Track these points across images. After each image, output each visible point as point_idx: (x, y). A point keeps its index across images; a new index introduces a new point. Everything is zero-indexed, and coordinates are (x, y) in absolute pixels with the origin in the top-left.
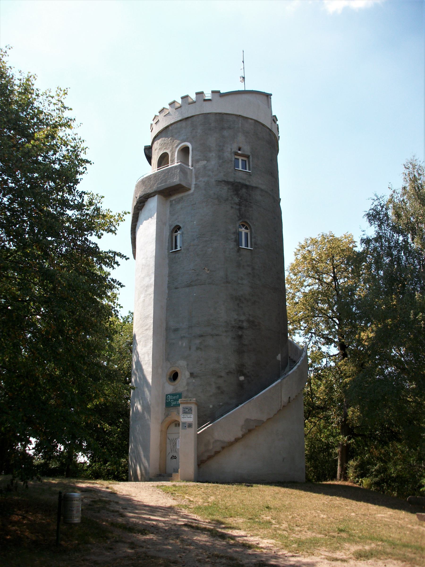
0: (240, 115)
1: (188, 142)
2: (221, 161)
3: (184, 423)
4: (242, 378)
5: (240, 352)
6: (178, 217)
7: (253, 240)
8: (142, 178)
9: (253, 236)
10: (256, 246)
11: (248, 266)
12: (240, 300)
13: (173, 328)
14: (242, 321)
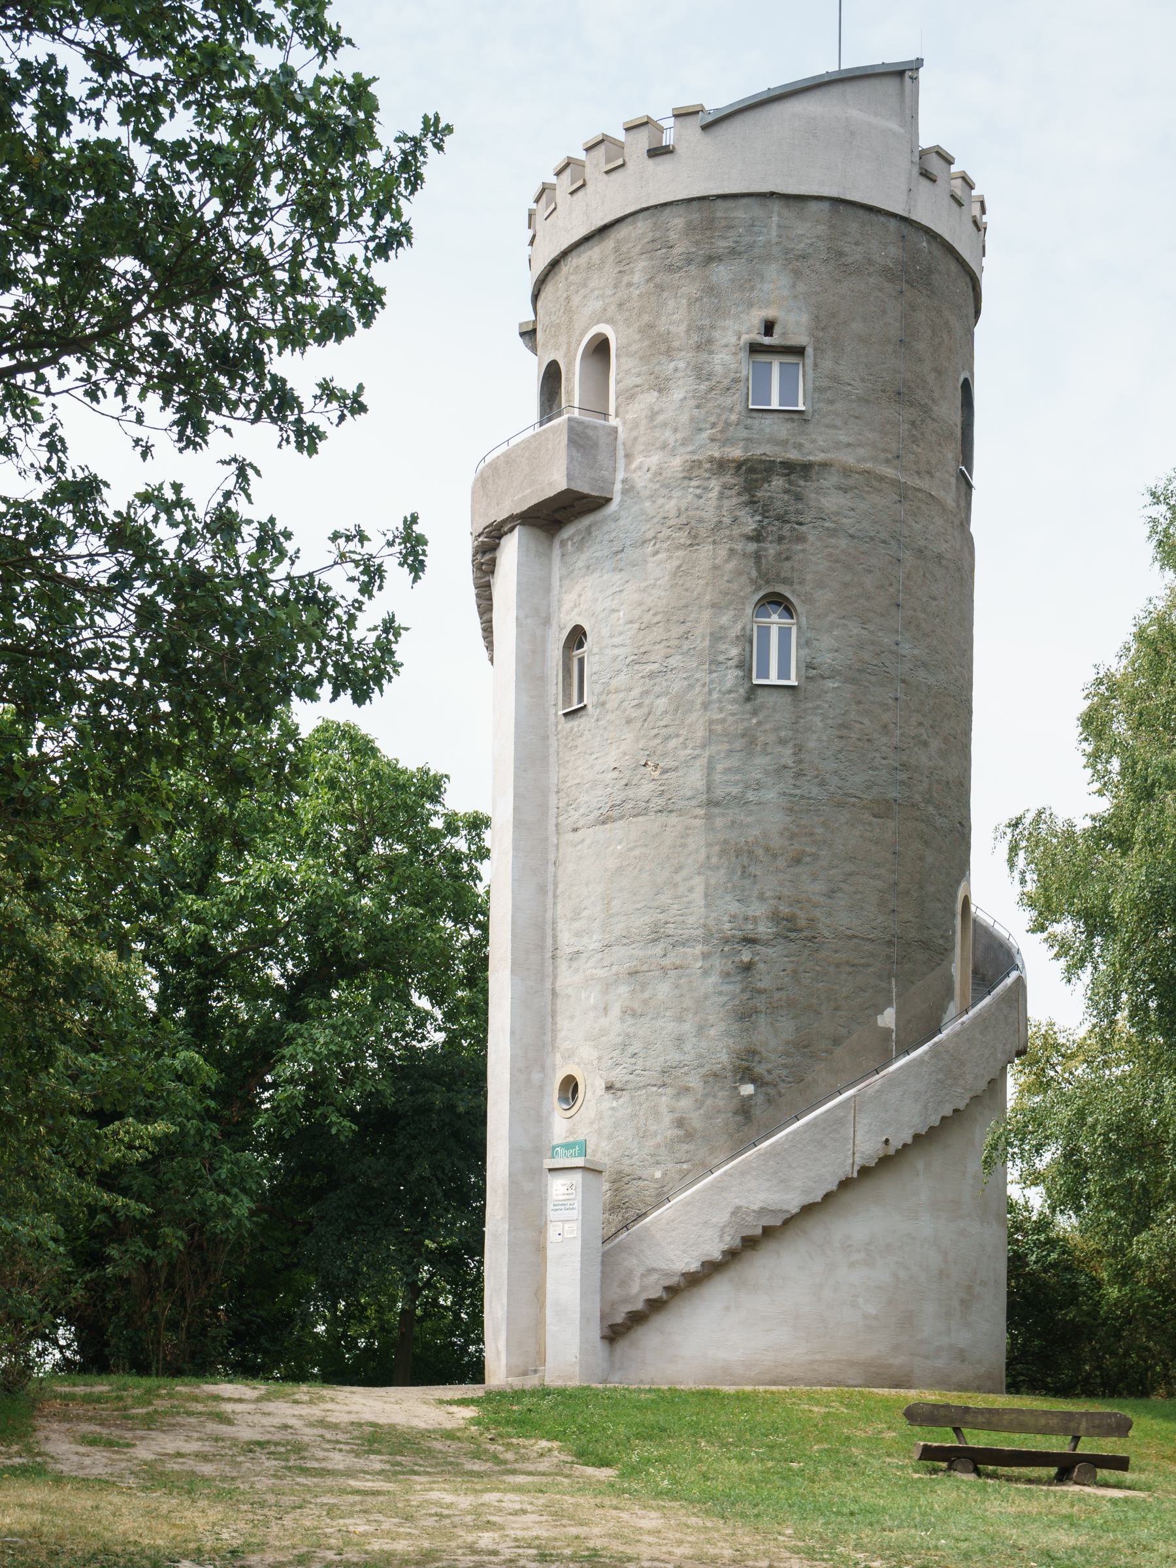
0: (772, 194)
1: (607, 322)
4: (748, 1089)
5: (745, 1016)
6: (580, 596)
8: (504, 448)
11: (782, 742)
12: (751, 852)
14: (755, 920)
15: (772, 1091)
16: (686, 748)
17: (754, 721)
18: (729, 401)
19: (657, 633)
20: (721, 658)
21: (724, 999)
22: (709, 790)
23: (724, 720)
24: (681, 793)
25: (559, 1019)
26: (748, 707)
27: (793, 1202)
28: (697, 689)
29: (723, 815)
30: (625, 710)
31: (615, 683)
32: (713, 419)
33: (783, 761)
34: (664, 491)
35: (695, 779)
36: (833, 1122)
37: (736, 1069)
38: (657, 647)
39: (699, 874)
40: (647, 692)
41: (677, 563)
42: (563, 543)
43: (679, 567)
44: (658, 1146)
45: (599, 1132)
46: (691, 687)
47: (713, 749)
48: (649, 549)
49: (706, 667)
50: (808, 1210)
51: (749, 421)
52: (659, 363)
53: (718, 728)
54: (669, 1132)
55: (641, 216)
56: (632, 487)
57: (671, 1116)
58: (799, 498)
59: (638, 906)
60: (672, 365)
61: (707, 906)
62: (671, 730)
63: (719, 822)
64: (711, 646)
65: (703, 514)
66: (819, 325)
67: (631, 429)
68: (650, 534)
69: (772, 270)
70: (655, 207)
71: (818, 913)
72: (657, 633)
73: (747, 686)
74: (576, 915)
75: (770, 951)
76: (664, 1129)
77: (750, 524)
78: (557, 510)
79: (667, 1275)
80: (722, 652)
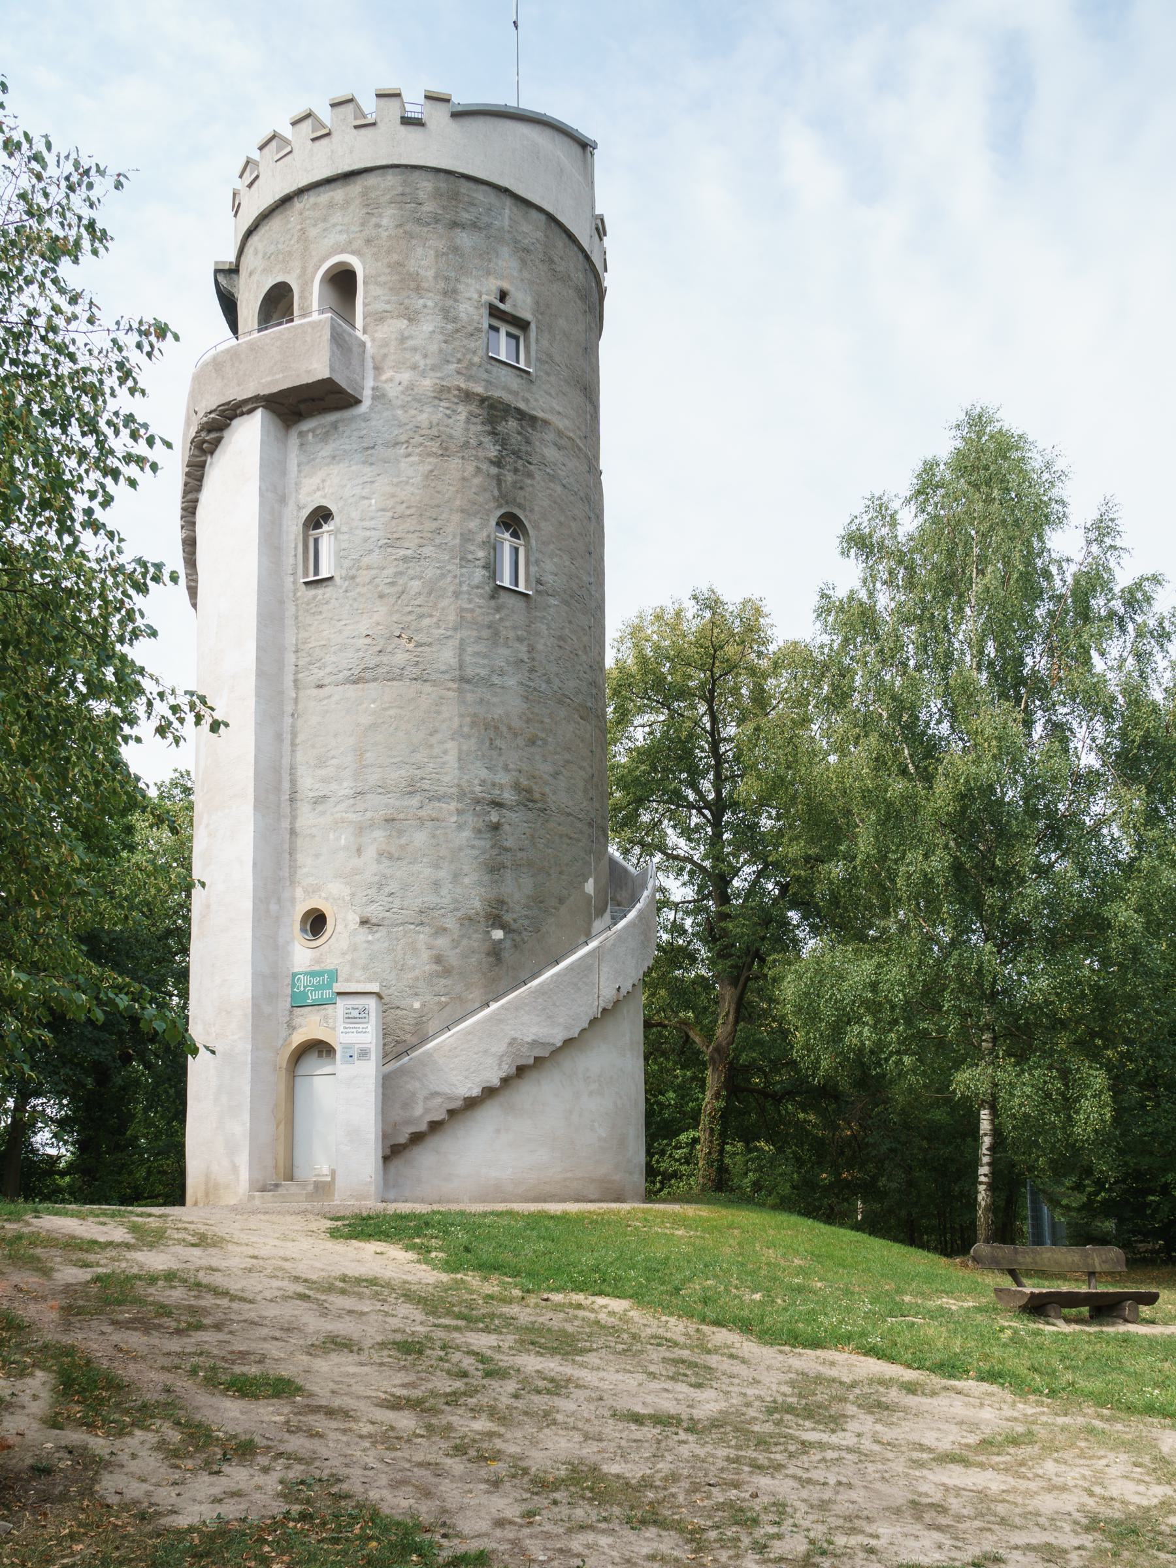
1: (353, 253)
3: (347, 1047)
4: (498, 934)
5: (494, 869)
6: (323, 481)
7: (533, 569)
8: (213, 352)
9: (532, 559)
10: (541, 588)
11: (519, 639)
12: (496, 728)
13: (311, 794)
14: (501, 787)
16: (439, 627)
17: (498, 617)
18: (472, 345)
19: (410, 524)
20: (470, 557)
21: (476, 852)
22: (461, 668)
23: (472, 611)
24: (435, 666)
25: (300, 858)
26: (493, 603)
27: (557, 1036)
28: (449, 580)
29: (473, 692)
30: (377, 586)
31: (366, 560)
32: (459, 356)
33: (521, 656)
34: (416, 405)
35: (447, 656)
36: (582, 968)
37: (488, 916)
38: (410, 536)
39: (453, 739)
40: (401, 573)
41: (430, 468)
42: (301, 434)
43: (432, 471)
44: (417, 979)
45: (353, 963)
46: (443, 576)
47: (464, 633)
48: (402, 450)
49: (457, 561)
50: (568, 1042)
51: (489, 367)
52: (408, 297)
53: (468, 616)
54: (428, 967)
55: (391, 171)
56: (384, 395)
57: (429, 952)
58: (528, 442)
59: (395, 760)
60: (421, 302)
61: (460, 768)
62: (424, 610)
63: (470, 697)
64: (462, 545)
65: (454, 433)
66: (540, 307)
67: (381, 347)
68: (403, 438)
69: (505, 251)
70: (406, 166)
71: (547, 790)
72: (410, 524)
73: (492, 585)
74: (321, 762)
75: (514, 815)
76: (423, 964)
77: (493, 451)
78: (304, 401)
79: (450, 1098)
80: (471, 552)
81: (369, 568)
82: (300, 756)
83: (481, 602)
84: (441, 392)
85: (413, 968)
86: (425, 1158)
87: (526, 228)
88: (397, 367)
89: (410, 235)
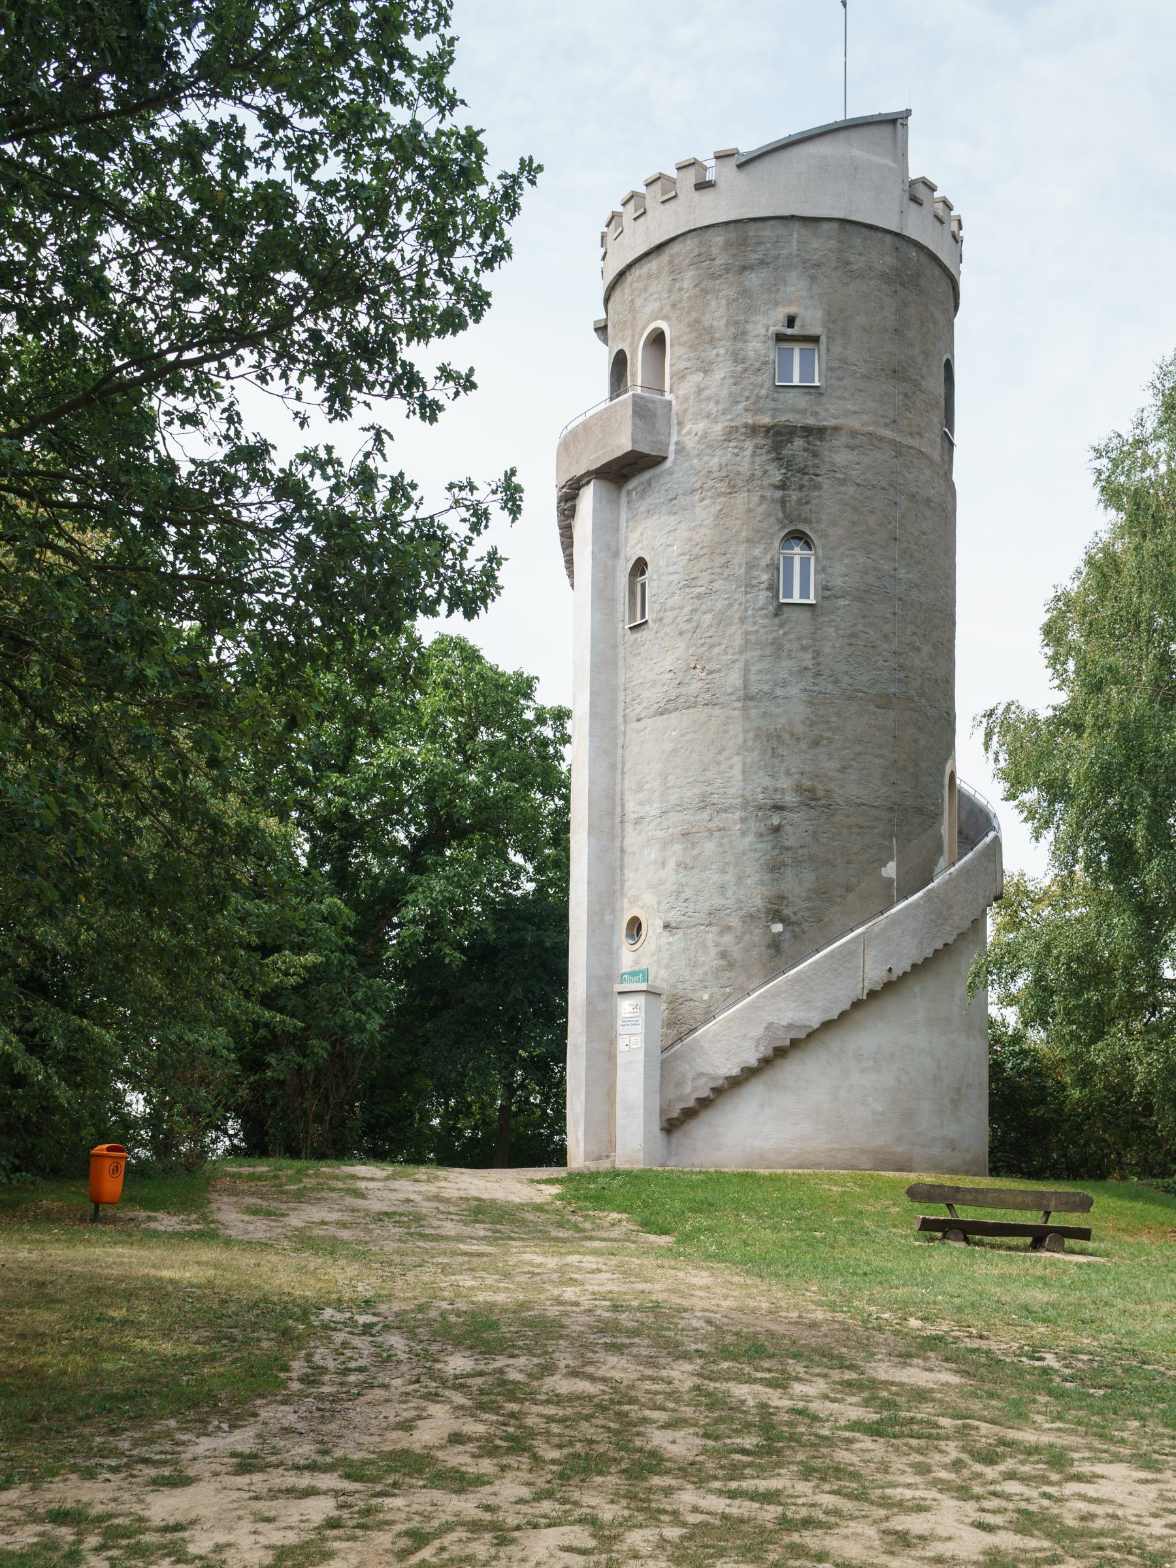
0: (793, 217)
1: (663, 319)
2: (739, 368)
4: (778, 928)
5: (775, 868)
8: (582, 419)
11: (804, 649)
12: (779, 737)
14: (783, 791)
15: (797, 929)
18: (760, 379)
19: (703, 563)
20: (754, 582)
21: (758, 855)
22: (745, 687)
23: (757, 632)
25: (626, 871)
26: (776, 620)
27: (815, 1020)
31: (670, 602)
32: (747, 394)
33: (805, 664)
34: (709, 451)
35: (734, 678)
36: (847, 954)
40: (695, 610)
42: (629, 493)
45: (659, 962)
46: (731, 605)
47: (748, 655)
48: (697, 497)
50: (827, 1025)
58: (815, 455)
61: (744, 780)
63: (753, 713)
64: (747, 573)
65: (740, 469)
66: (830, 318)
68: (698, 485)
69: (793, 276)
71: (833, 786)
72: (703, 563)
74: (640, 788)
75: (795, 816)
76: (711, 959)
77: (777, 476)
81: (672, 609)
82: (627, 785)
83: (765, 621)
84: (731, 432)
85: (704, 964)
86: (699, 1131)
87: (816, 243)
88: (695, 420)
89: (705, 292)
